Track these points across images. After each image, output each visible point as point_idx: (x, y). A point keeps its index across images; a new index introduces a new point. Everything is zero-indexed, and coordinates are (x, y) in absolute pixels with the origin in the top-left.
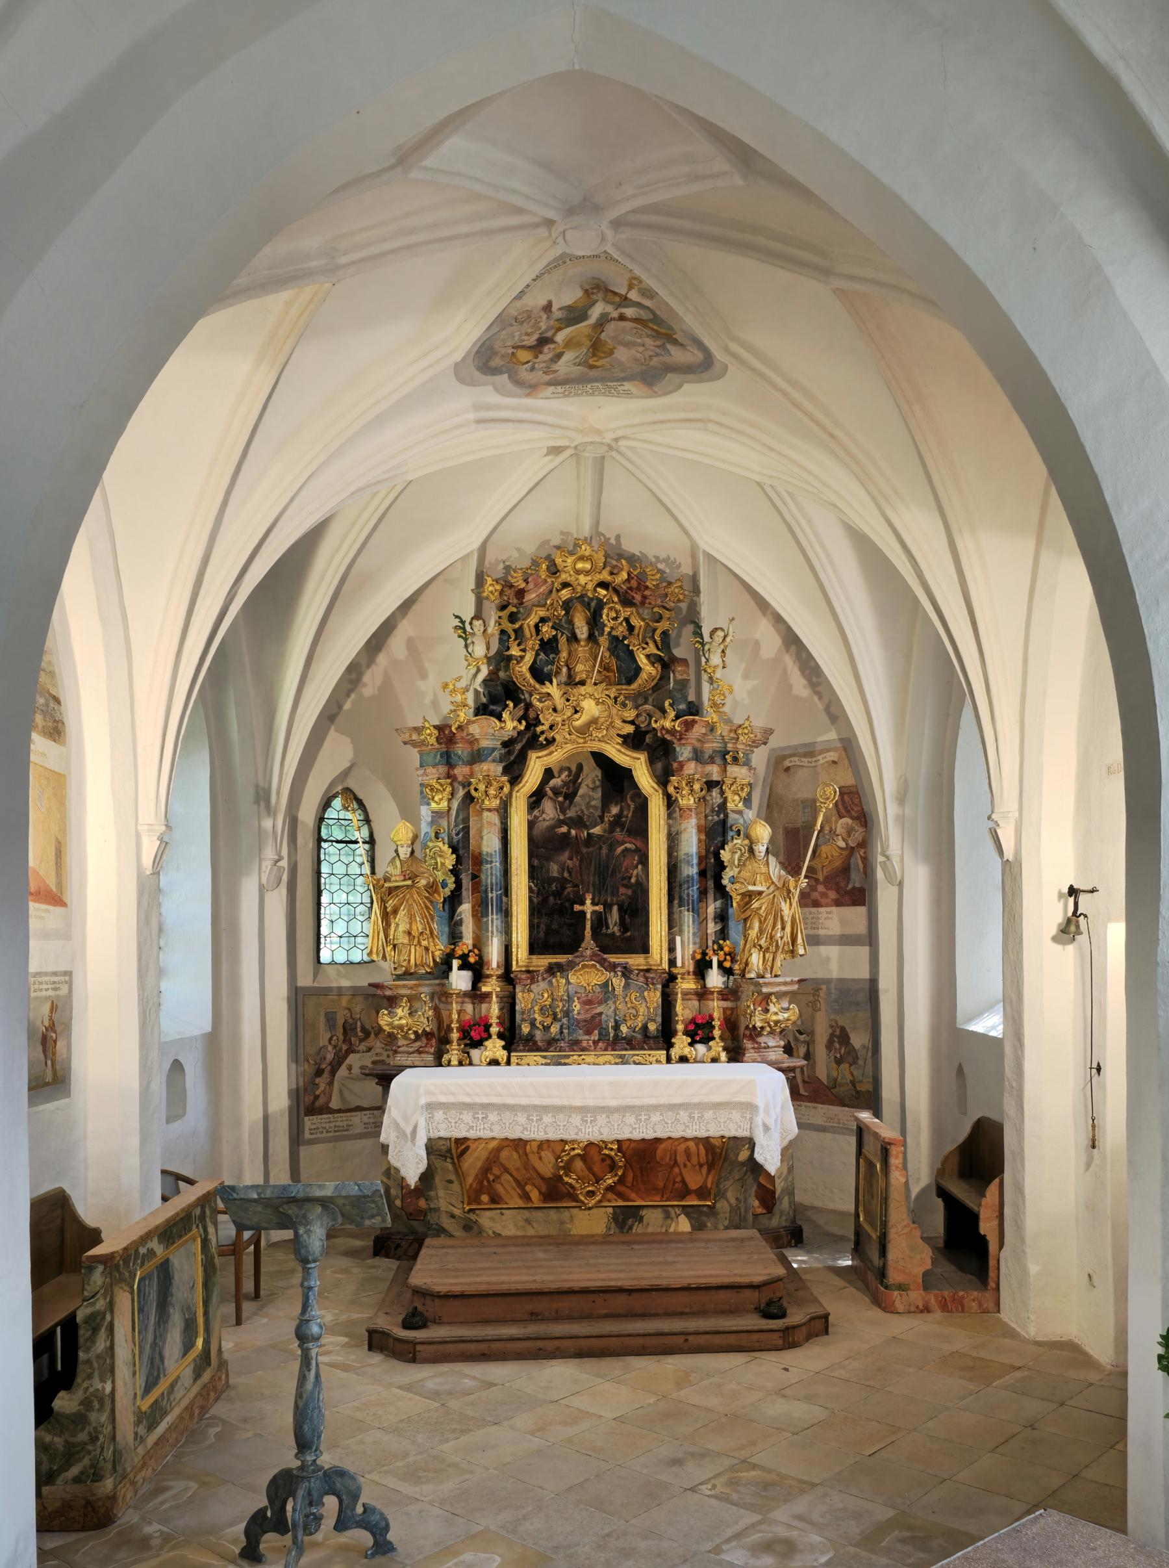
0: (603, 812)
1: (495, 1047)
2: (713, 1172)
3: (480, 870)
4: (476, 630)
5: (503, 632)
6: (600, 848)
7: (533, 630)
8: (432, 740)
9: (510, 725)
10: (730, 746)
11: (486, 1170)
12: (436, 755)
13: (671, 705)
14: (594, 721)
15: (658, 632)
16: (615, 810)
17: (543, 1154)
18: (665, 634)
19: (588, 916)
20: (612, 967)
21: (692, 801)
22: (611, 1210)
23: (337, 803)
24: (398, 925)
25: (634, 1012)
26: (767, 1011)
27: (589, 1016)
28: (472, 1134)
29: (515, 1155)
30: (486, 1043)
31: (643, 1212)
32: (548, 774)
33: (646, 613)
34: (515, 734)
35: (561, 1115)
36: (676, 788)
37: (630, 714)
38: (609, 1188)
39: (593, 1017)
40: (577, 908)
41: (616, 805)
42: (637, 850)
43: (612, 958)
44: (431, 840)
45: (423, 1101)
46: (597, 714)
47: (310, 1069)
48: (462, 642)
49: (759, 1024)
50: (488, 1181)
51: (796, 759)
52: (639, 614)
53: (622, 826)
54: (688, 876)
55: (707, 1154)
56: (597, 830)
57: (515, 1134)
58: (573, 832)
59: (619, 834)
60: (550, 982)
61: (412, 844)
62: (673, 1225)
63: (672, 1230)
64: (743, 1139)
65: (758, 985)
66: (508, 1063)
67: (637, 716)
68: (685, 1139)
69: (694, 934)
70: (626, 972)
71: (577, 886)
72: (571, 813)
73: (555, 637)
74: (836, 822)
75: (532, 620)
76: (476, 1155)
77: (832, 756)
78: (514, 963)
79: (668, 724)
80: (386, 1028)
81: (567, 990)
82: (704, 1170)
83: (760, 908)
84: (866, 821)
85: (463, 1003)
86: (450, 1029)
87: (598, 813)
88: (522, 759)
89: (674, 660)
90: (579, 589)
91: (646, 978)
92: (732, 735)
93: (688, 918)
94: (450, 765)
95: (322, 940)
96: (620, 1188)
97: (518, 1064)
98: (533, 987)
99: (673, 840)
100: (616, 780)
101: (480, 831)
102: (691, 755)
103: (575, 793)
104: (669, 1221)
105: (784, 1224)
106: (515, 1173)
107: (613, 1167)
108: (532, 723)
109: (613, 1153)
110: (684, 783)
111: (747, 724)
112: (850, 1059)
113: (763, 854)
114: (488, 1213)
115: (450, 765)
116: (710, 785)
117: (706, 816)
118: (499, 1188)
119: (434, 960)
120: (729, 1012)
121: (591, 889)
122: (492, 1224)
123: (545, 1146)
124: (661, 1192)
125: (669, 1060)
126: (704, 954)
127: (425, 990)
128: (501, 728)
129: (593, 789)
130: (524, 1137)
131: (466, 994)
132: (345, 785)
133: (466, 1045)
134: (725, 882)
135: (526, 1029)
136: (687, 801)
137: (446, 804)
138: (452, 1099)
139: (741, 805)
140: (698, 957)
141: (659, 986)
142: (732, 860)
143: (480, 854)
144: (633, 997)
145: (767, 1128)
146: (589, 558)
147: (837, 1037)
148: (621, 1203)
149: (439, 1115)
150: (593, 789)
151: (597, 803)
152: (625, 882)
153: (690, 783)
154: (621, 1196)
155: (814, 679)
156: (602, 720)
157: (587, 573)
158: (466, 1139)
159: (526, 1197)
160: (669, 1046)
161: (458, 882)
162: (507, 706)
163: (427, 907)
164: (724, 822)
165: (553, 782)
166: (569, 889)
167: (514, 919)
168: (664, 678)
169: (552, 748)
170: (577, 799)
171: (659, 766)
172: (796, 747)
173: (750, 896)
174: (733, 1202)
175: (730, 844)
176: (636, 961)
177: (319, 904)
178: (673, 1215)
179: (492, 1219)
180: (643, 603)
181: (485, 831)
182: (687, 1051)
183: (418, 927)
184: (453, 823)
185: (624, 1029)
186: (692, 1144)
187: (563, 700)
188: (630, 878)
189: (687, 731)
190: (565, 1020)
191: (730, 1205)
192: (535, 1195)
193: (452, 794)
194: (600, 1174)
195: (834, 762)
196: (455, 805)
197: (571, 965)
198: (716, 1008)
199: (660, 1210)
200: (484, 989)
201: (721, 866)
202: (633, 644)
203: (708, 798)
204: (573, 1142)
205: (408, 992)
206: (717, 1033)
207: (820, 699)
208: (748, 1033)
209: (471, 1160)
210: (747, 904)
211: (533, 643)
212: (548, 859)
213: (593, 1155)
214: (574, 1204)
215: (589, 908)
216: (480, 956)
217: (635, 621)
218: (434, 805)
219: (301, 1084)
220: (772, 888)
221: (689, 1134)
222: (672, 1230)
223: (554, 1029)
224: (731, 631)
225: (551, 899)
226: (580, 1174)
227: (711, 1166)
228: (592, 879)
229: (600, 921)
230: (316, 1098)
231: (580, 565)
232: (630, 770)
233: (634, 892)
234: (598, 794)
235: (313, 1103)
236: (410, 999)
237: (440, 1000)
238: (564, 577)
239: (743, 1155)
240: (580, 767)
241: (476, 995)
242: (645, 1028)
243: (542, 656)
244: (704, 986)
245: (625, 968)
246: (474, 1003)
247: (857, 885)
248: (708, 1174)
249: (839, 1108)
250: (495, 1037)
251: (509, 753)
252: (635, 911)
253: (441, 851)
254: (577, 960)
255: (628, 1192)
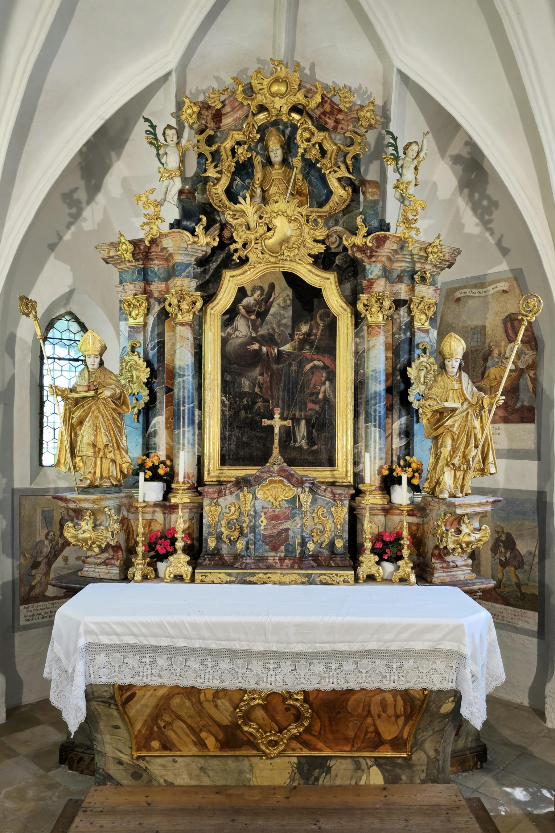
0: (293, 331)
1: (179, 562)
2: (410, 723)
3: (173, 384)
4: (169, 140)
5: (200, 155)
6: (290, 365)
7: (229, 153)
8: (129, 256)
9: (205, 241)
10: (418, 266)
11: (155, 717)
12: (133, 272)
13: (364, 221)
14: (285, 240)
15: (350, 156)
16: (304, 328)
17: (219, 702)
18: (356, 158)
19: (277, 431)
20: (300, 483)
21: (381, 318)
22: (295, 760)
23: (61, 325)
24: (83, 436)
25: (321, 527)
26: (459, 532)
27: (275, 531)
28: (138, 681)
29: (188, 703)
30: (171, 558)
31: (331, 763)
32: (242, 292)
33: (338, 138)
34: (209, 251)
35: (240, 661)
36: (365, 305)
37: (321, 234)
38: (295, 738)
39: (280, 533)
40: (266, 422)
41: (306, 323)
42: (325, 367)
43: (299, 471)
44: (127, 354)
45: (82, 642)
46: (289, 233)
47: (26, 562)
48: (154, 151)
49: (451, 546)
50: (159, 728)
51: (467, 290)
52: (331, 139)
53: (311, 344)
54: (376, 392)
55: (405, 707)
56: (287, 348)
57: (187, 681)
58: (264, 349)
59: (307, 352)
60: (238, 496)
61: (101, 354)
62: (364, 777)
63: (362, 783)
64: (448, 692)
65: (453, 505)
66: (192, 580)
67: (328, 236)
68: (381, 691)
69: (380, 449)
70: (314, 487)
71: (267, 401)
72: (262, 331)
73: (250, 159)
74: (506, 346)
75: (228, 144)
76: (143, 701)
77: (503, 286)
78: (206, 473)
79: (359, 240)
80: (72, 540)
81: (254, 505)
82: (401, 721)
83: (453, 425)
84: (536, 345)
85: (154, 512)
86: (137, 543)
87: (289, 331)
88: (217, 278)
89: (363, 182)
90: (274, 112)
91: (334, 494)
92: (422, 253)
93: (375, 433)
94: (147, 282)
95: (45, 445)
96: (306, 737)
97: (202, 581)
98: (221, 500)
99: (360, 359)
100: (307, 298)
101: (174, 345)
102: (381, 273)
103: (267, 311)
104: (359, 773)
105: (469, 745)
106: (188, 721)
107: (298, 717)
108: (225, 243)
109: (298, 704)
110: (373, 300)
111: (437, 242)
112: (516, 564)
113: (456, 370)
114: (159, 760)
115: (147, 282)
116: (398, 303)
117: (393, 335)
118: (171, 735)
119: (121, 472)
120: (414, 528)
121: (281, 403)
122: (163, 772)
123: (221, 694)
124: (351, 742)
125: (356, 579)
126: (391, 470)
127: (110, 503)
128: (194, 242)
129: (284, 308)
130: (196, 684)
131: (156, 505)
132: (68, 310)
133: (152, 558)
134: (411, 399)
135: (212, 543)
136: (375, 317)
137: (142, 319)
138: (115, 640)
139: (427, 324)
140: (386, 473)
141: (347, 503)
142: (418, 378)
143: (174, 368)
144: (320, 513)
145: (474, 677)
146: (285, 81)
147: (503, 542)
148: (306, 753)
149: (101, 658)
150: (284, 308)
151: (287, 321)
152: (313, 398)
153: (380, 301)
154: (306, 745)
155: (487, 217)
156: (294, 239)
157: (282, 96)
158: (130, 686)
159: (202, 744)
160: (355, 565)
161: (153, 396)
162: (200, 220)
163: (114, 419)
164: (411, 340)
165: (246, 301)
166: (260, 404)
167: (207, 431)
168: (355, 200)
169: (246, 267)
170: (269, 317)
171: (348, 286)
172: (467, 280)
173: (442, 413)
174: (432, 754)
175: (417, 362)
176: (321, 474)
177: (41, 414)
178: (364, 766)
179: (164, 766)
180: (335, 128)
181: (178, 346)
182: (374, 569)
183: (102, 440)
184: (149, 338)
185: (311, 547)
186: (389, 698)
187: (256, 217)
188: (318, 394)
189: (378, 247)
190: (251, 536)
191: (428, 757)
192: (211, 742)
193: (148, 310)
194: (284, 723)
195: (505, 292)
196: (151, 320)
197: (259, 480)
198: (403, 523)
199: (349, 760)
200: (173, 500)
201: (408, 383)
202: (325, 165)
203: (396, 317)
204: (253, 691)
205: (91, 506)
206: (406, 552)
207: (492, 234)
208: (436, 552)
209: (138, 707)
210: (438, 421)
211: (228, 164)
212: (240, 375)
213: (277, 706)
214: (254, 753)
215: (277, 423)
216: (172, 468)
217: (329, 146)
218: (131, 321)
219: (17, 576)
220: (466, 405)
221: (387, 685)
222: (362, 783)
223: (240, 546)
224: (425, 147)
225: (243, 412)
226: (261, 722)
227: (408, 717)
228: (281, 393)
229: (288, 435)
230: (32, 588)
231: (275, 88)
232: (320, 290)
233: (322, 408)
234: (289, 313)
235: (29, 592)
236: (94, 513)
237: (128, 511)
238: (260, 99)
239: (447, 707)
240: (272, 287)
241: (166, 505)
242: (332, 544)
243: (238, 181)
244: (390, 502)
245: (313, 484)
246: (164, 513)
247: (526, 404)
248: (405, 725)
249: (503, 607)
250: (180, 552)
251: (205, 272)
252: (322, 425)
253: (136, 364)
254: (265, 476)
255: (314, 741)
